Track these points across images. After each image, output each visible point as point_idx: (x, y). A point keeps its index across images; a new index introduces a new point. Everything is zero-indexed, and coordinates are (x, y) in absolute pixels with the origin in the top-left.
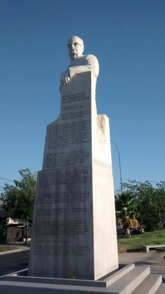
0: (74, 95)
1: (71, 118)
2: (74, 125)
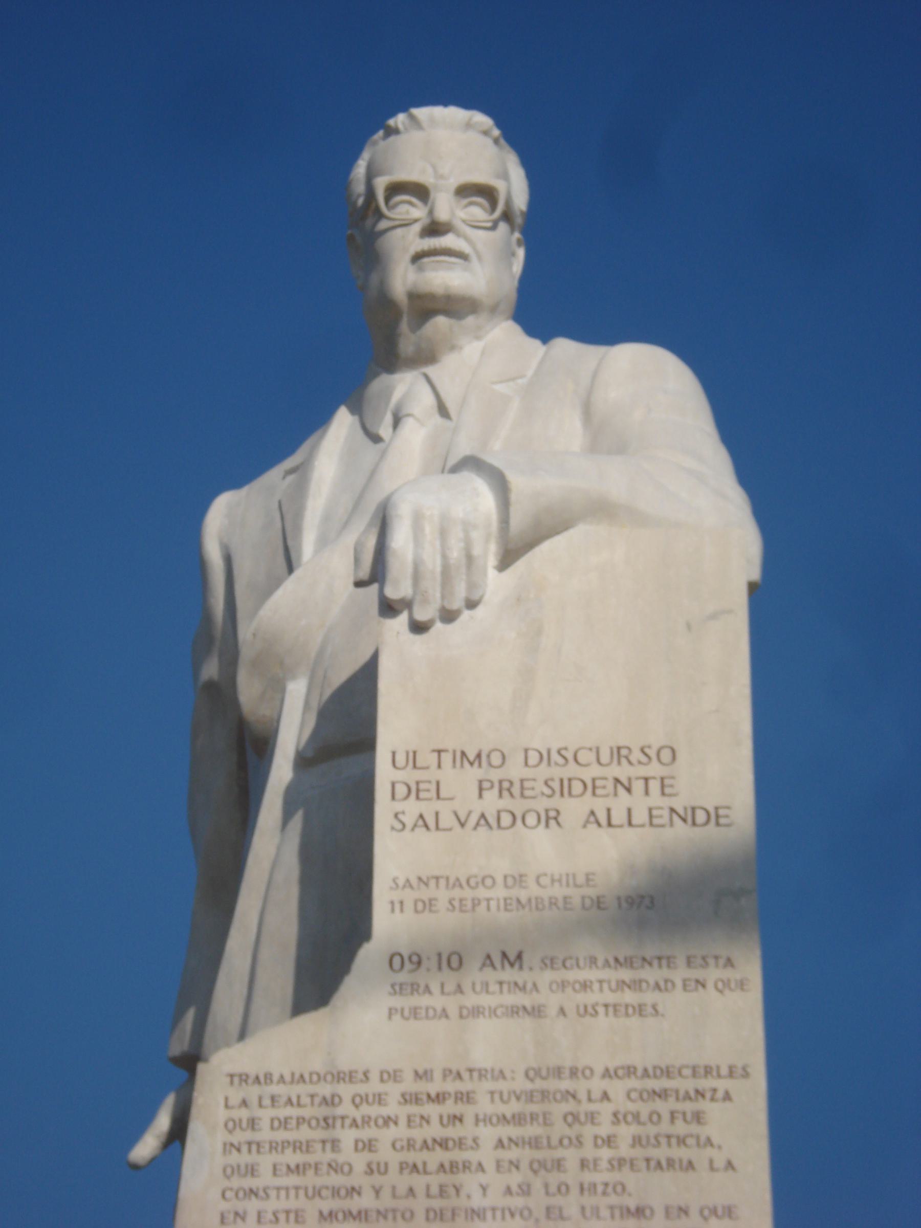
0: (545, 757)
1: (514, 1011)
2: (545, 1095)
